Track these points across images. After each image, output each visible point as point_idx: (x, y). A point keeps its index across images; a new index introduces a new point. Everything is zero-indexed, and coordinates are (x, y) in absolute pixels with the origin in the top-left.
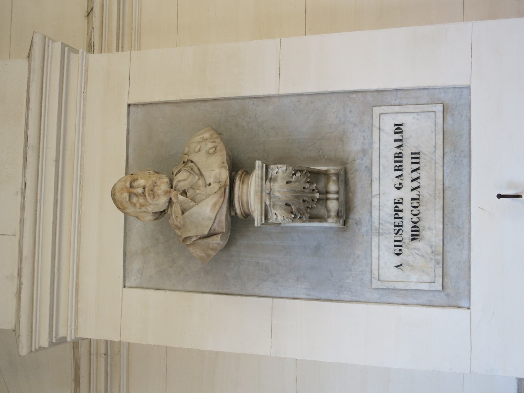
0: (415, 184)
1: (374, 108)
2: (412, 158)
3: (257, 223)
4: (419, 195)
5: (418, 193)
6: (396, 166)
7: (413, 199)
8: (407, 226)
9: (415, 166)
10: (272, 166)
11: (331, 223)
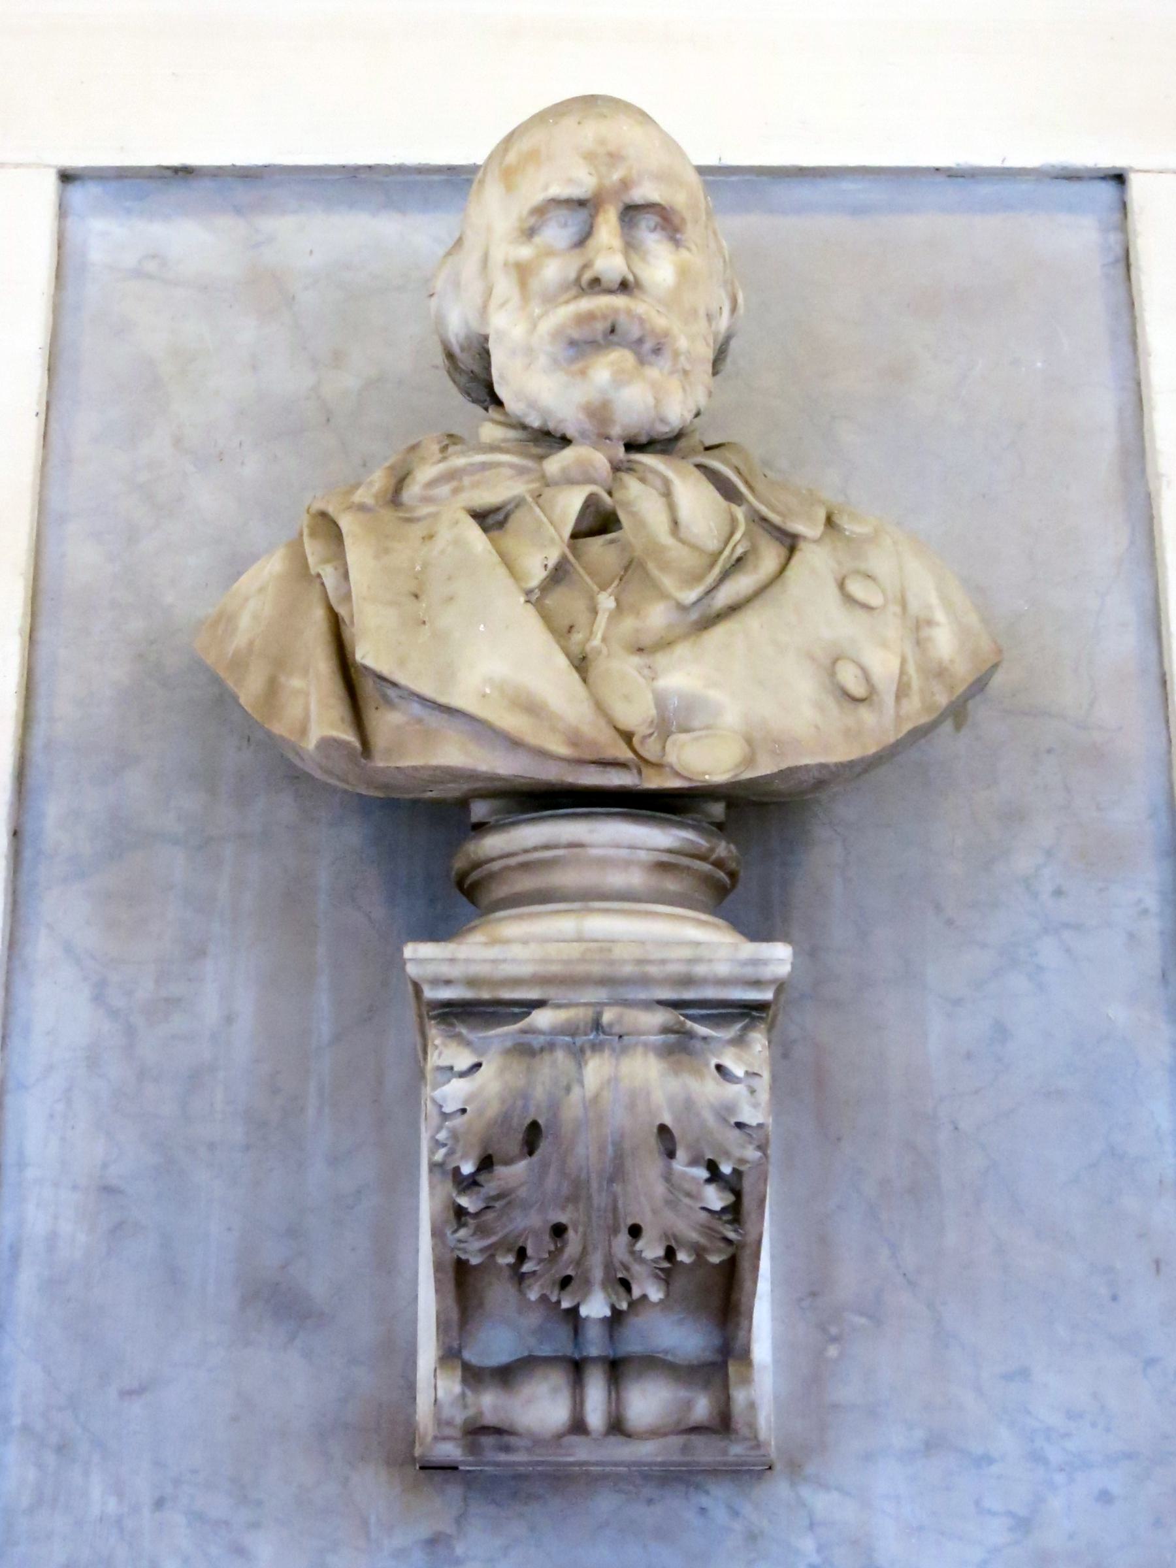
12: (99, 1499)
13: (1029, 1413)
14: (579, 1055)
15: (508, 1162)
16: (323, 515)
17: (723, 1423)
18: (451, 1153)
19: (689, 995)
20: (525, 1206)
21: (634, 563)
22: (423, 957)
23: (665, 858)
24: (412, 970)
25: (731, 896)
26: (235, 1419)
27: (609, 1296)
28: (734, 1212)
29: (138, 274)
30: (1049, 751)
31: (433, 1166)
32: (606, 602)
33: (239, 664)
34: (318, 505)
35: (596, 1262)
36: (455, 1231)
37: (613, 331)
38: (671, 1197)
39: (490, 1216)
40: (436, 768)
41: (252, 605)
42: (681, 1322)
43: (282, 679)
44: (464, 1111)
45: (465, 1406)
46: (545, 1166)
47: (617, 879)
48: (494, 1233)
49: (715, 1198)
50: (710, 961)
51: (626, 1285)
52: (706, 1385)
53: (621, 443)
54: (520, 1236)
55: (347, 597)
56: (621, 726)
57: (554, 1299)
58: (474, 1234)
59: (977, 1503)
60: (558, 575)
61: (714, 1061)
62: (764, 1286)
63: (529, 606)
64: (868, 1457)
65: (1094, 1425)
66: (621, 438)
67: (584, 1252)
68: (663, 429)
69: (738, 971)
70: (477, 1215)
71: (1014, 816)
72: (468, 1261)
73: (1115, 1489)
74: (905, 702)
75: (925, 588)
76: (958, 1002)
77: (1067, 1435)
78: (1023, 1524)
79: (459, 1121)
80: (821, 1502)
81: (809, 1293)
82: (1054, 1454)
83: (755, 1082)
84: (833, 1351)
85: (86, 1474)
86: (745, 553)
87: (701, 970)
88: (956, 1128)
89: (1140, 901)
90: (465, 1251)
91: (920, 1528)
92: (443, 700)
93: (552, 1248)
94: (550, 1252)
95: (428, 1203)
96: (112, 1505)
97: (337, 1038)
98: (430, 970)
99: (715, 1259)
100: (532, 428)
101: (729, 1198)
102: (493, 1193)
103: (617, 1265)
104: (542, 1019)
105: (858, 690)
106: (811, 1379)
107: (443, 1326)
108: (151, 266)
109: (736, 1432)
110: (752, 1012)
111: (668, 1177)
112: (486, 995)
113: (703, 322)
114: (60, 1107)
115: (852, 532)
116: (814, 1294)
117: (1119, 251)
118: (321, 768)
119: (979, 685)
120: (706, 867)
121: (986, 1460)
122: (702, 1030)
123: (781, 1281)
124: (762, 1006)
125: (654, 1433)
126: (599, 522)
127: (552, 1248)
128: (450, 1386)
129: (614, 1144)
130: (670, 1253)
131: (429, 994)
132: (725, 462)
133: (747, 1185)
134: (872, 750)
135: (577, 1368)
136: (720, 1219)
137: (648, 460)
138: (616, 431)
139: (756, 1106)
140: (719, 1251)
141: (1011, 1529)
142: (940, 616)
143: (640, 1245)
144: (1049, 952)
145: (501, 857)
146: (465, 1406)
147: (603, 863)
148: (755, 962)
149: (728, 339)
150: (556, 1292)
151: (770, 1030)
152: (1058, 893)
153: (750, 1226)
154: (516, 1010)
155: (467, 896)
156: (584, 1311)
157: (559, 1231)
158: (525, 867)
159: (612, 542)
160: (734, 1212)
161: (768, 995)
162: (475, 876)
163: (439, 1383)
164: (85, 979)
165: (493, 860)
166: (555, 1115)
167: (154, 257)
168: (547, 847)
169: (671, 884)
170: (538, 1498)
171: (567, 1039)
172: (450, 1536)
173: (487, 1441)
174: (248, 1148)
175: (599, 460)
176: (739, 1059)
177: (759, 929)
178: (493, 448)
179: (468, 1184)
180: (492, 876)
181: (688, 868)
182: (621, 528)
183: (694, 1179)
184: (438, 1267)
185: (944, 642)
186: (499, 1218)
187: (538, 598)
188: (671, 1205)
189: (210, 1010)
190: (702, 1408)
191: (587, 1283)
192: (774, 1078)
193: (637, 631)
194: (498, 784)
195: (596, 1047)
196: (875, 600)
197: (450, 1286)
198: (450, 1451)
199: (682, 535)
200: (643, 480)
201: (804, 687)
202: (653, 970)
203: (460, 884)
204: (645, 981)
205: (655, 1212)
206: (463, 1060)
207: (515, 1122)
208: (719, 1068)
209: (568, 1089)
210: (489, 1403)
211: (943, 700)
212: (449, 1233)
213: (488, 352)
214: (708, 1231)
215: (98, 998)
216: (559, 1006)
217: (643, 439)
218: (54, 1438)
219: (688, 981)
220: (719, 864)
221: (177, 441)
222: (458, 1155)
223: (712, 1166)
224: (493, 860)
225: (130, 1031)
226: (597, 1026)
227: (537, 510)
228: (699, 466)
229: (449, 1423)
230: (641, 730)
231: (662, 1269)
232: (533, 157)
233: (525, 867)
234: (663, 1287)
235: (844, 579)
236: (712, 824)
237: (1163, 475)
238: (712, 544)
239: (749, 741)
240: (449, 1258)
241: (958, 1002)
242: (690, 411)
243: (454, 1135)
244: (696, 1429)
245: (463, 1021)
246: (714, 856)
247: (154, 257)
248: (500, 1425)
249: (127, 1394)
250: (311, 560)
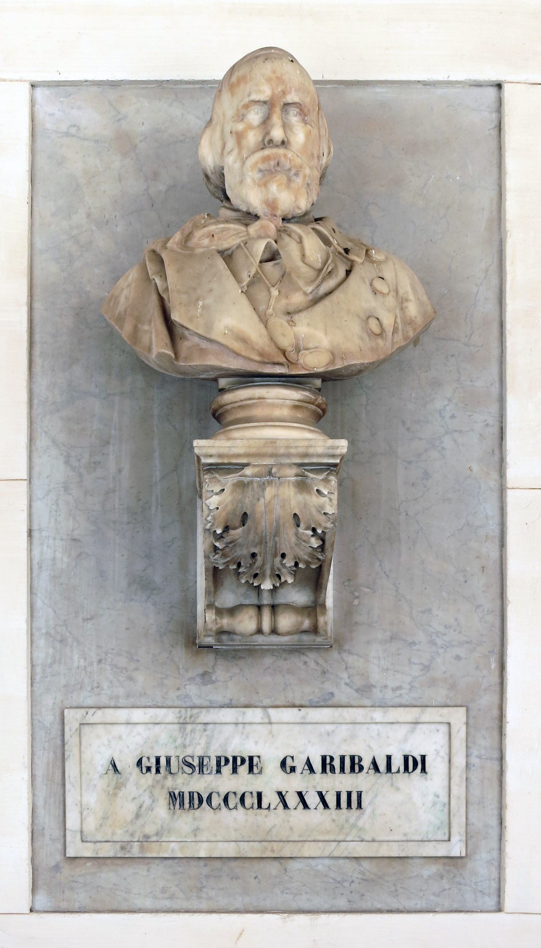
0: (292, 800)
2: (349, 794)
6: (332, 759)
7: (260, 795)
9: (331, 800)
12: (77, 660)
13: (431, 626)
14: (263, 486)
15: (235, 528)
16: (154, 251)
17: (315, 630)
18: (213, 525)
19: (306, 461)
20: (241, 546)
21: (286, 273)
22: (201, 445)
23: (297, 403)
24: (196, 451)
25: (322, 419)
26: (127, 629)
27: (272, 581)
28: (322, 548)
29: (67, 134)
30: (452, 356)
31: (205, 530)
32: (275, 292)
33: (120, 320)
34: (153, 247)
35: (268, 568)
36: (214, 556)
37: (278, 164)
38: (298, 542)
39: (227, 550)
40: (206, 365)
41: (126, 292)
42: (299, 591)
43: (140, 326)
44: (218, 508)
45: (217, 624)
46: (249, 530)
47: (277, 413)
48: (229, 557)
49: (315, 543)
50: (315, 447)
51: (279, 577)
52: (309, 616)
53: (281, 218)
54: (239, 558)
55: (167, 289)
56: (281, 348)
57: (251, 582)
58: (221, 557)
59: (409, 660)
60: (255, 280)
61: (316, 488)
62: (331, 577)
63: (243, 294)
64: (368, 642)
65: (455, 631)
66: (281, 216)
67: (263, 565)
68: (299, 212)
69: (326, 451)
70: (222, 550)
71: (436, 384)
72: (218, 567)
73: (462, 655)
74: (396, 335)
75: (406, 282)
76: (410, 462)
77: (445, 634)
78: (426, 668)
79: (216, 512)
80: (351, 659)
81: (348, 580)
82: (439, 642)
83: (332, 496)
84: (356, 602)
85: (72, 651)
86: (332, 269)
87: (311, 451)
88: (407, 514)
89: (486, 420)
90: (217, 563)
91: (387, 669)
92: (208, 336)
93: (251, 562)
94: (250, 564)
95: (202, 544)
96: (82, 662)
97: (163, 478)
98: (204, 451)
99: (314, 567)
100: (243, 211)
101: (321, 543)
102: (229, 541)
103: (276, 569)
104: (248, 471)
105: (377, 330)
106: (347, 613)
107: (208, 593)
108: (73, 131)
109: (319, 633)
110: (331, 468)
111: (297, 534)
112: (226, 461)
113: (316, 160)
114: (54, 507)
115: (376, 259)
116: (349, 580)
117: (495, 123)
118: (157, 365)
119: (426, 327)
120: (314, 407)
121: (414, 643)
122: (311, 475)
123: (337, 575)
124: (335, 465)
125: (288, 633)
126: (272, 256)
127: (251, 562)
128: (211, 616)
129: (276, 521)
130: (296, 564)
131: (204, 460)
132: (326, 227)
133: (327, 537)
134: (382, 357)
135: (259, 608)
136: (316, 551)
137: (294, 227)
138: (279, 213)
139: (331, 506)
140: (315, 563)
141: (421, 670)
142: (411, 297)
143: (284, 562)
144: (447, 442)
145: (231, 403)
146: (217, 624)
147: (273, 405)
148: (333, 447)
149: (326, 167)
150: (252, 579)
151: (337, 474)
152: (453, 417)
153: (328, 554)
154: (238, 467)
155: (218, 419)
156: (262, 587)
157: (254, 555)
158: (242, 407)
159: (277, 264)
160: (322, 548)
161: (338, 461)
162: (220, 411)
163: (207, 615)
164: (61, 454)
165: (228, 404)
166: (254, 510)
167: (74, 126)
168: (250, 399)
169: (299, 415)
170: (244, 658)
171: (258, 479)
172: (211, 673)
173: (224, 637)
174: (128, 523)
175: (272, 228)
176: (325, 487)
177: (332, 434)
178: (227, 221)
179: (219, 538)
180: (227, 411)
181: (307, 408)
182: (281, 258)
183: (307, 535)
184: (207, 570)
185: (412, 310)
186: (231, 550)
187: (247, 293)
188: (297, 544)
189: (112, 467)
190: (307, 623)
191: (264, 576)
192: (339, 494)
193: (288, 304)
194: (230, 372)
195: (270, 483)
196: (385, 290)
197: (211, 578)
198: (210, 640)
199: (306, 261)
200: (289, 235)
201: (355, 327)
202: (293, 451)
203: (214, 415)
204: (289, 455)
205: (291, 548)
206: (217, 489)
207: (238, 513)
208: (317, 490)
209: (258, 500)
210: (225, 622)
211: (411, 334)
212: (211, 557)
213: (223, 175)
214: (312, 556)
215: (67, 463)
216: (255, 466)
217: (290, 216)
218: (59, 637)
219: (306, 455)
220: (318, 406)
221: (89, 215)
222: (216, 526)
223: (314, 530)
224: (228, 404)
225: (80, 475)
226: (270, 473)
227: (246, 250)
228: (313, 229)
229: (210, 630)
230: (289, 349)
231: (293, 571)
232: (243, 79)
233: (242, 407)
234: (293, 578)
235: (373, 280)
236: (316, 389)
237: (508, 231)
238: (319, 265)
239: (333, 354)
240: (211, 566)
241: (410, 462)
242: (310, 203)
243: (214, 518)
244: (305, 632)
245: (217, 472)
246: (317, 403)
247: (74, 126)
248: (229, 631)
249: (85, 620)
250: (150, 272)
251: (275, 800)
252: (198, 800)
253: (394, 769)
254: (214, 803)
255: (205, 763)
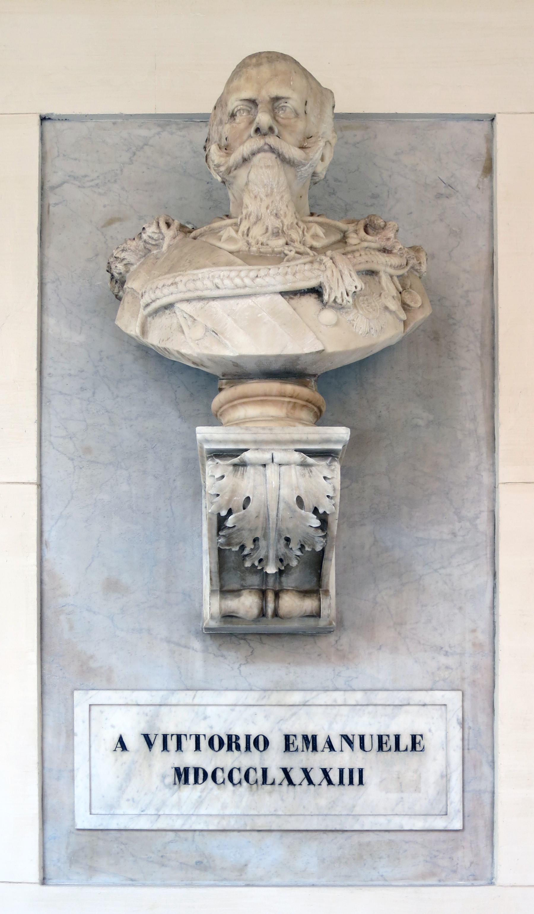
0: (297, 776)
1: (76, 693)
2: (351, 771)
3: (203, 432)
4: (273, 783)
5: (277, 782)
6: (237, 738)
7: (265, 771)
8: (207, 760)
9: (335, 777)
10: (337, 466)
11: (211, 606)
17: (317, 615)
251: (280, 776)
252: (200, 775)
253: (402, 747)
254: (219, 779)
255: (417, 741)
